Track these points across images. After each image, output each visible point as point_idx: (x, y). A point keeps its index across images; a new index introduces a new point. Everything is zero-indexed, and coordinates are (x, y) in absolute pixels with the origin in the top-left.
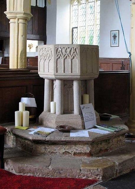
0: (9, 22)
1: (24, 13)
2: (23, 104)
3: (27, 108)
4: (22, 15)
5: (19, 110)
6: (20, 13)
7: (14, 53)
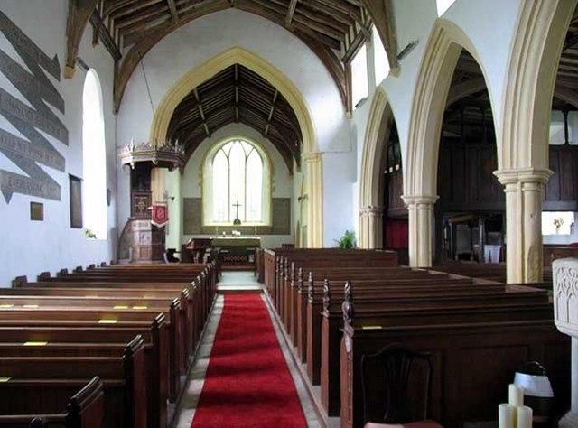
0: (505, 191)
1: (534, 172)
2: (518, 390)
3: (528, 400)
4: (530, 175)
5: (507, 402)
6: (527, 172)
7: (515, 246)
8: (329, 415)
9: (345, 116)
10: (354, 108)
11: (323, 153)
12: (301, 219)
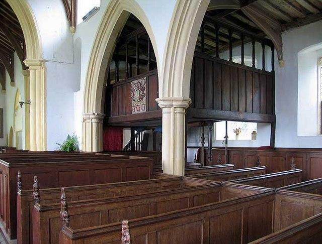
8: (11, 239)
9: (69, 31)
10: (79, 20)
11: (47, 61)
12: (14, 125)
